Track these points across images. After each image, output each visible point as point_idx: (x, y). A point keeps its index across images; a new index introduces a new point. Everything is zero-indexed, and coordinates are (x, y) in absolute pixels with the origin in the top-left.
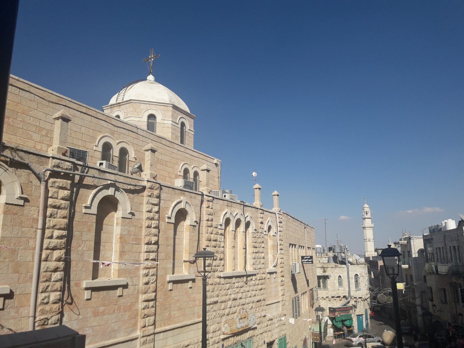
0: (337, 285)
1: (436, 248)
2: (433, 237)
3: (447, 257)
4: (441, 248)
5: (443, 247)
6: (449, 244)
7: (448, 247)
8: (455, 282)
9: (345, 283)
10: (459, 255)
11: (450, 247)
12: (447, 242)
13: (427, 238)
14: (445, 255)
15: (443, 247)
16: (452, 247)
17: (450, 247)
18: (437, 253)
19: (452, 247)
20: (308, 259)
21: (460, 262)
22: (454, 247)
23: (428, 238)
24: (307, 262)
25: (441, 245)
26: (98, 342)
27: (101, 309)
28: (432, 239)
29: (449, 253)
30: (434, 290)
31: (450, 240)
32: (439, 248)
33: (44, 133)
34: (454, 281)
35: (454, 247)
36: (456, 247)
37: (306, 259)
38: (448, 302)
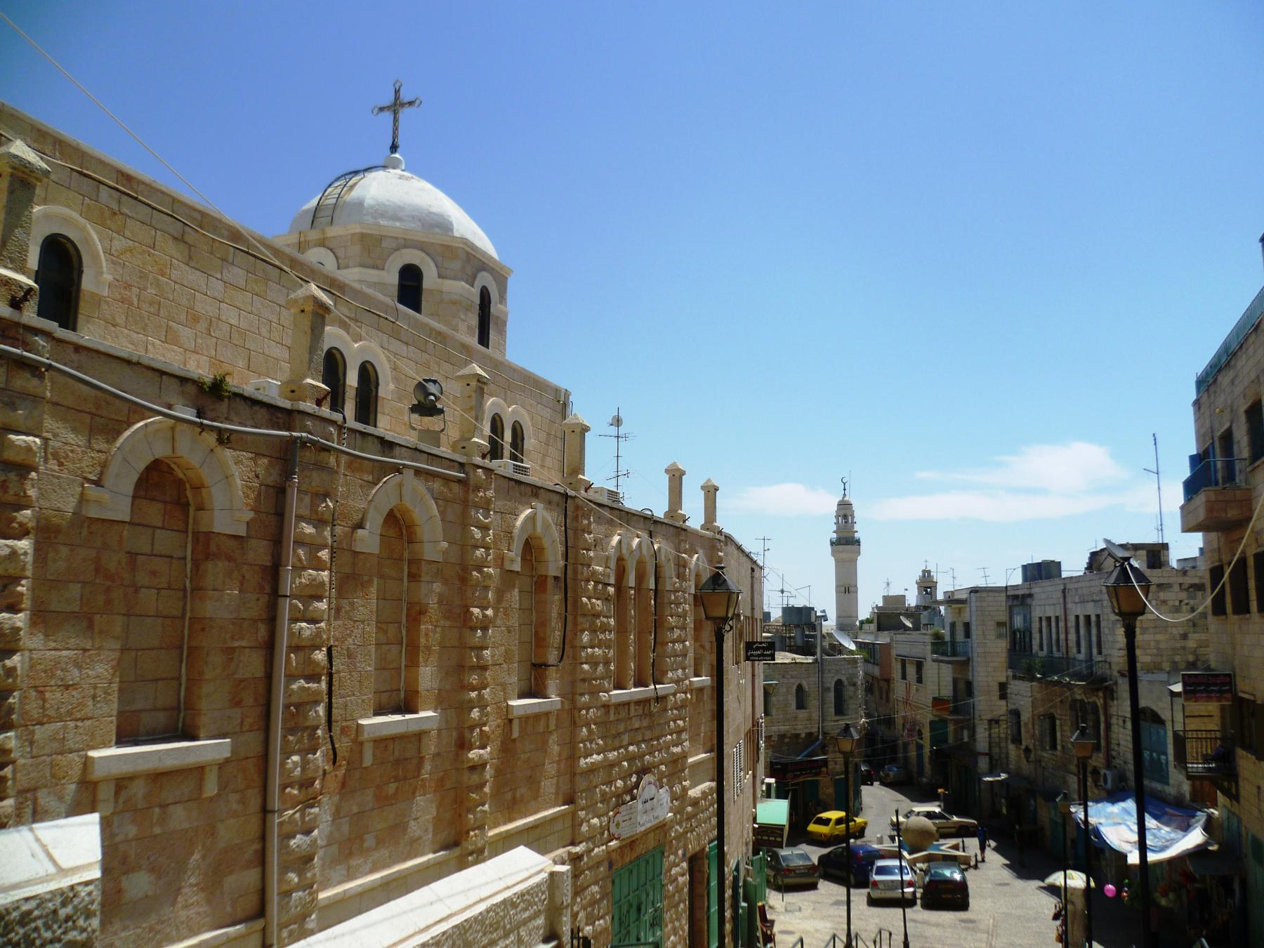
0: (794, 706)
1: (1041, 619)
2: (1033, 591)
3: (1067, 640)
4: (1053, 620)
5: (1057, 618)
6: (1076, 610)
7: (1072, 619)
8: (1082, 701)
9: (813, 703)
10: (1099, 636)
11: (1077, 617)
12: (1069, 606)
13: (1017, 593)
14: (1062, 636)
15: (1057, 618)
16: (1082, 619)
17: (1077, 617)
18: (1041, 631)
19: (1082, 619)
20: (764, 649)
21: (1100, 653)
22: (1088, 618)
23: (1020, 592)
24: (758, 656)
25: (1050, 612)
26: (488, 911)
27: (392, 788)
28: (1030, 596)
29: (1072, 631)
30: (1025, 717)
31: (1077, 599)
32: (1049, 619)
33: (202, 326)
34: (1078, 697)
35: (1088, 618)
36: (1093, 619)
37: (757, 649)
38: (1059, 747)
